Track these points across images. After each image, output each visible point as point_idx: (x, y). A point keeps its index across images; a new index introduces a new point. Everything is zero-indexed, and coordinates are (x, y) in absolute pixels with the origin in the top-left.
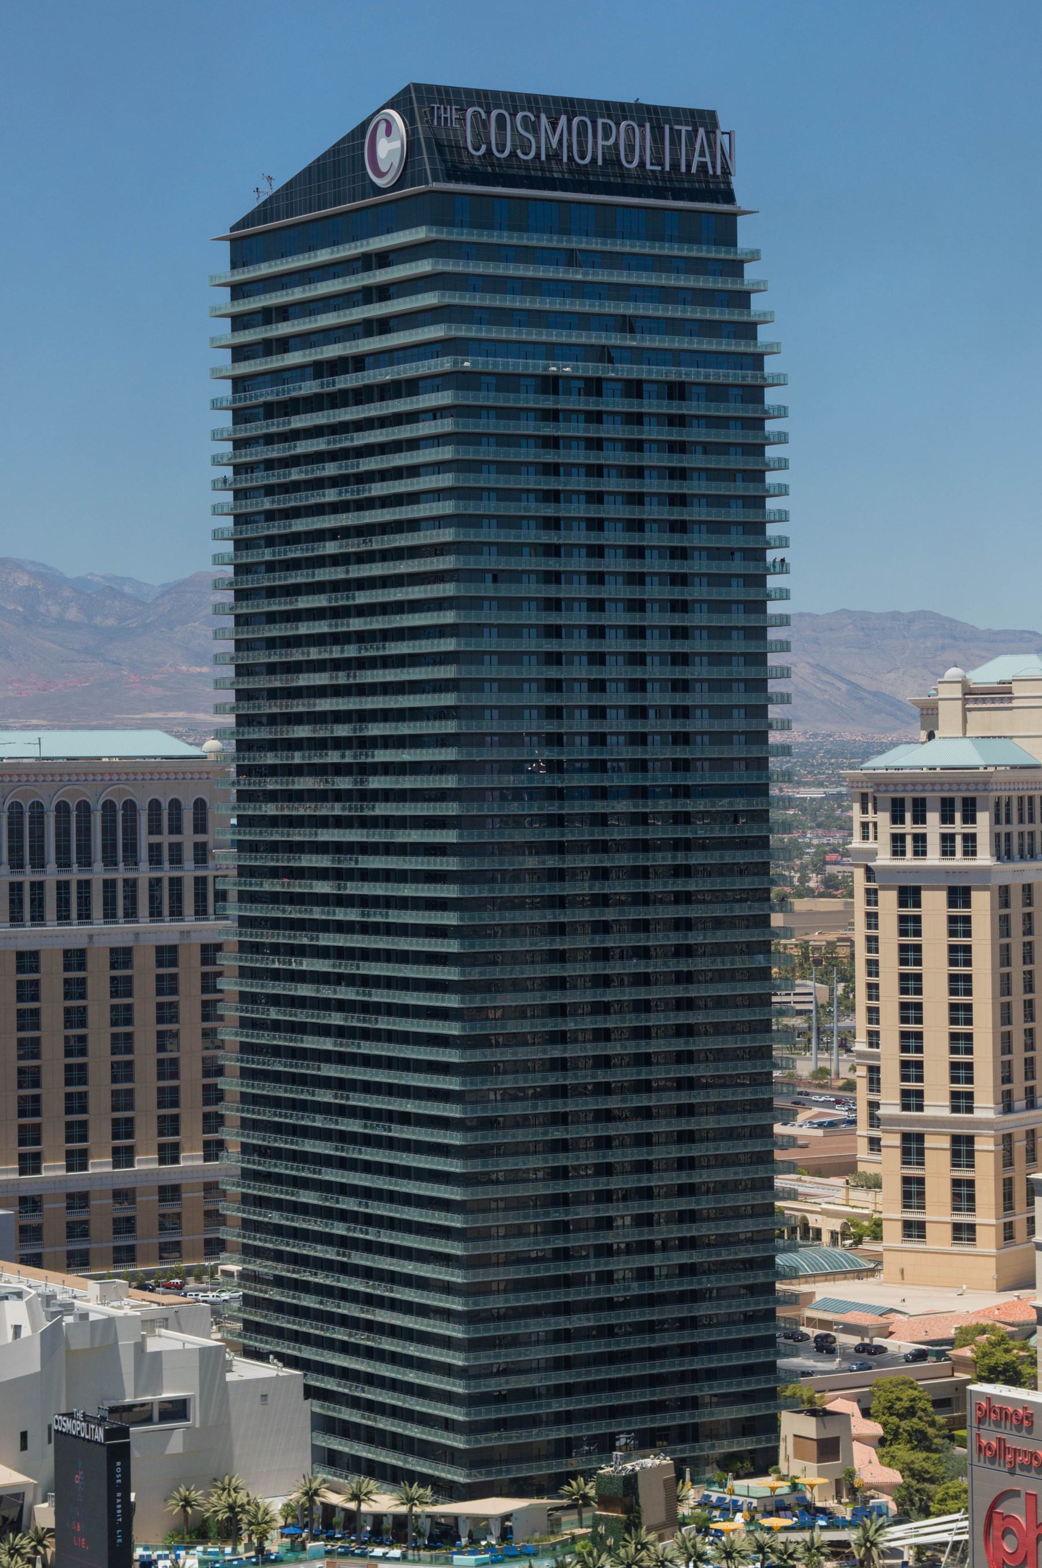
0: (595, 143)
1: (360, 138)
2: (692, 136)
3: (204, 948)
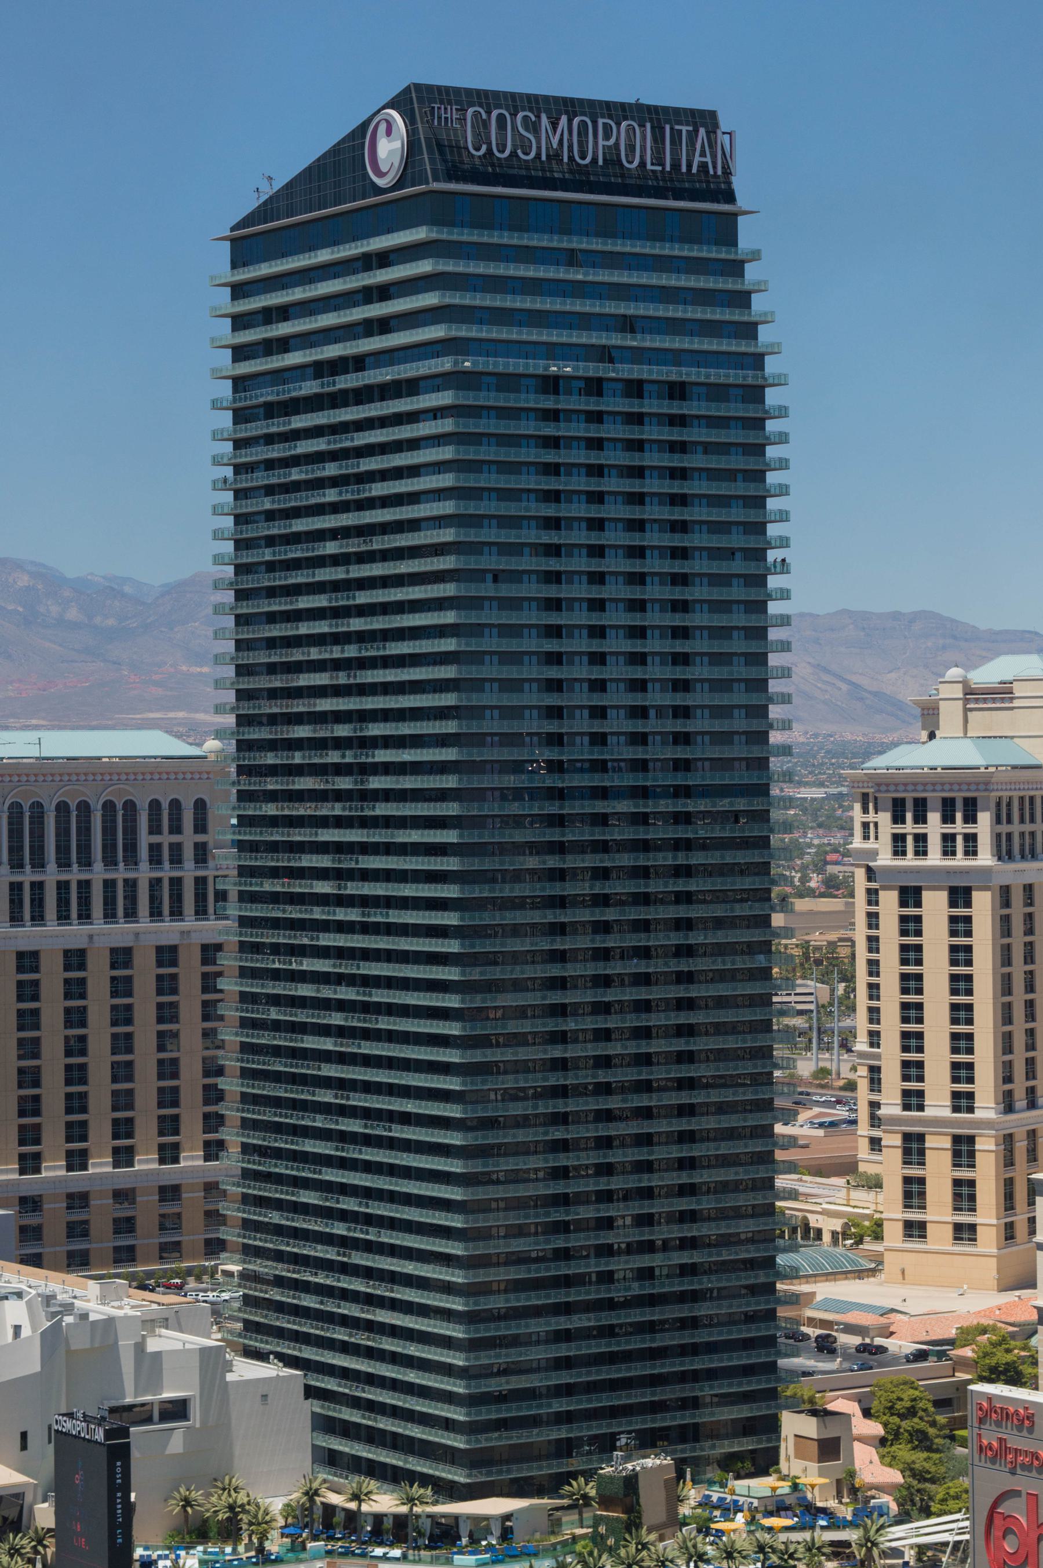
0: (596, 143)
1: (360, 138)
2: (693, 136)
3: (205, 948)
